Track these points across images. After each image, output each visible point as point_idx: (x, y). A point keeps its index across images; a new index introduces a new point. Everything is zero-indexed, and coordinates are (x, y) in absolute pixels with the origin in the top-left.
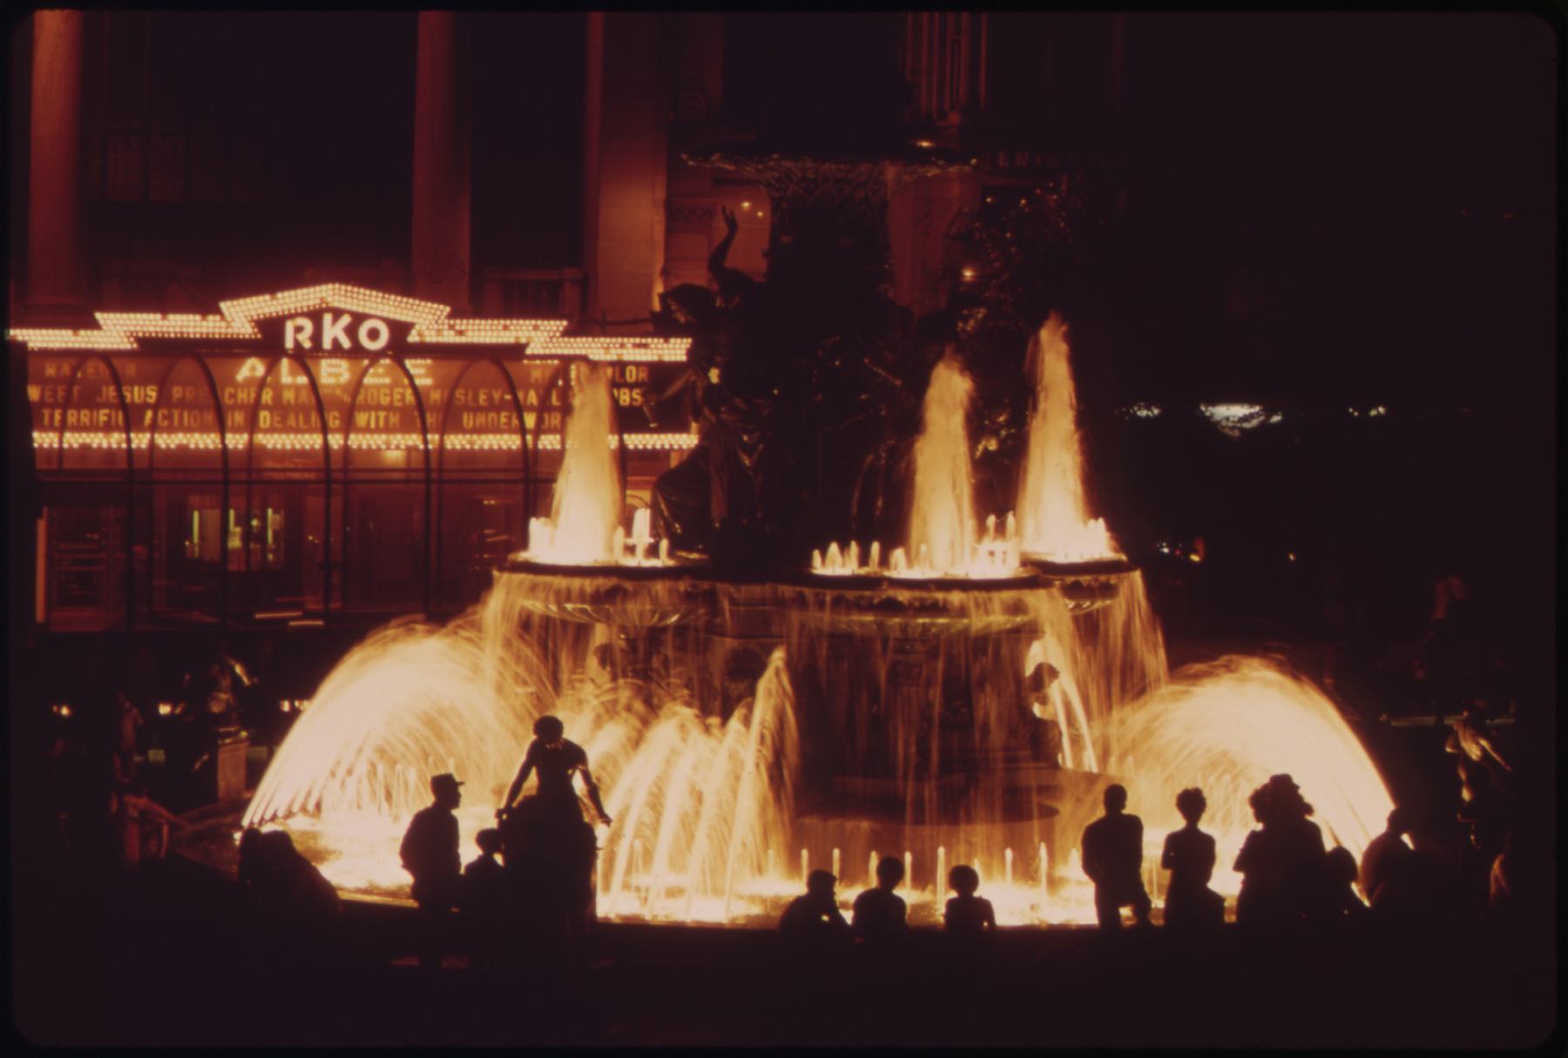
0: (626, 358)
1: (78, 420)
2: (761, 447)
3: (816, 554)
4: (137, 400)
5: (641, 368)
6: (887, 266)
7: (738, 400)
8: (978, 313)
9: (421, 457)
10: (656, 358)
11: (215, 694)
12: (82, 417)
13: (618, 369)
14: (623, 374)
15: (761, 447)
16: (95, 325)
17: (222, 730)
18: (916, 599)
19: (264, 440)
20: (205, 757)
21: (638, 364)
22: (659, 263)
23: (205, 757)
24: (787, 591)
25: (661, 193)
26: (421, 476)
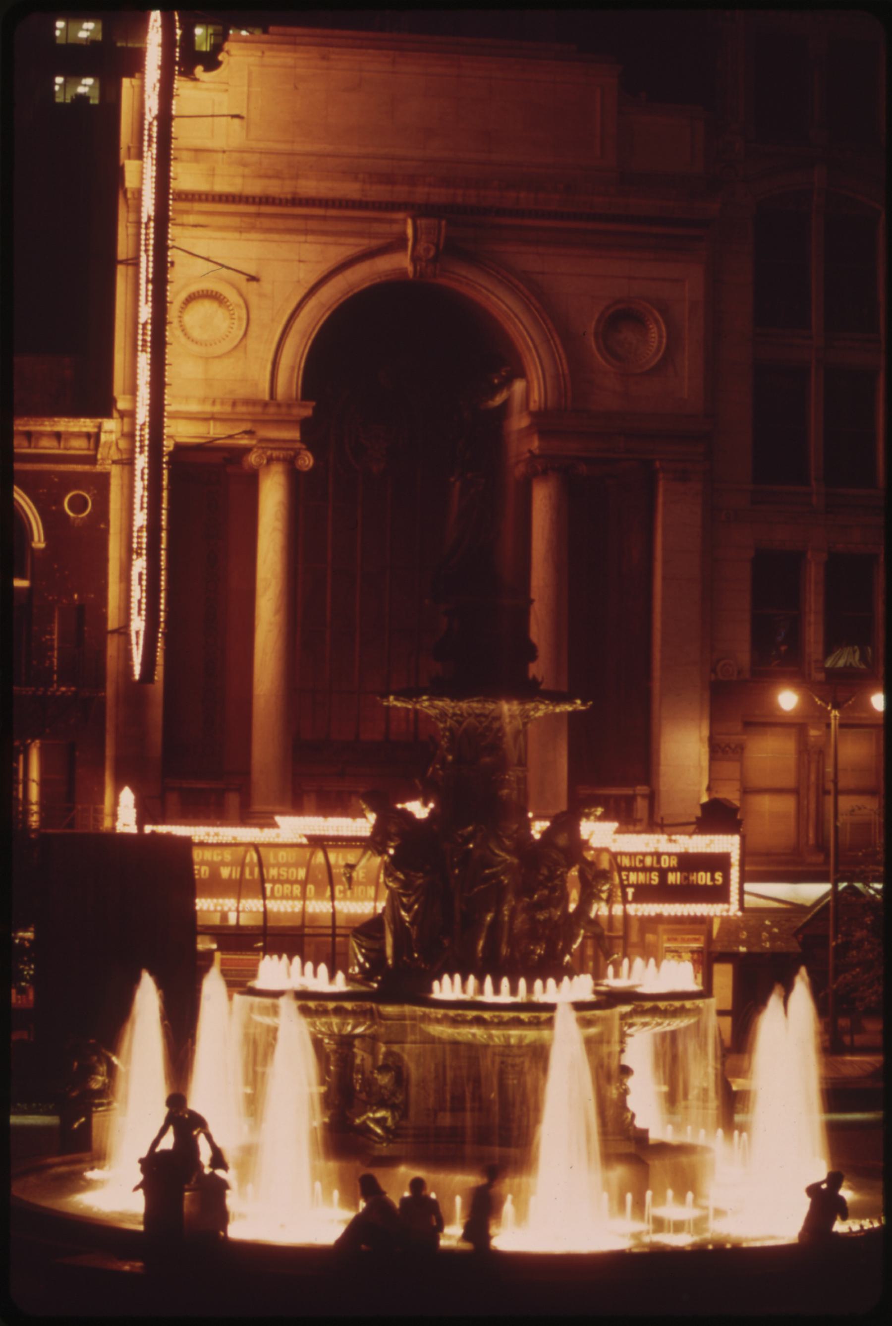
0: (661, 850)
1: (292, 892)
2: (416, 907)
3: (436, 984)
4: (700, 882)
5: (672, 857)
6: (507, 777)
7: (398, 873)
8: (596, 811)
9: (261, 917)
10: (683, 850)
11: (93, 1076)
12: (285, 889)
13: (655, 858)
14: (659, 862)
15: (416, 907)
16: (274, 825)
17: (97, 1101)
18: (495, 1016)
19: (274, 906)
20: (83, 1120)
21: (670, 854)
22: (705, 783)
23: (83, 1120)
24: (419, 1010)
25: (705, 732)
26: (330, 931)
